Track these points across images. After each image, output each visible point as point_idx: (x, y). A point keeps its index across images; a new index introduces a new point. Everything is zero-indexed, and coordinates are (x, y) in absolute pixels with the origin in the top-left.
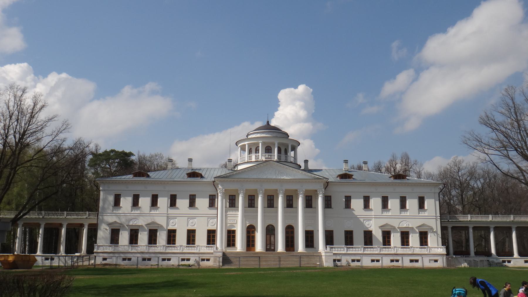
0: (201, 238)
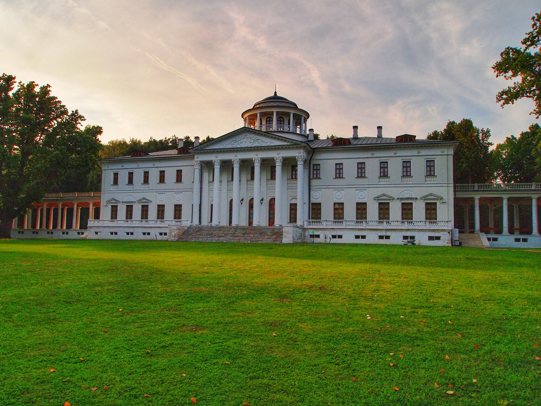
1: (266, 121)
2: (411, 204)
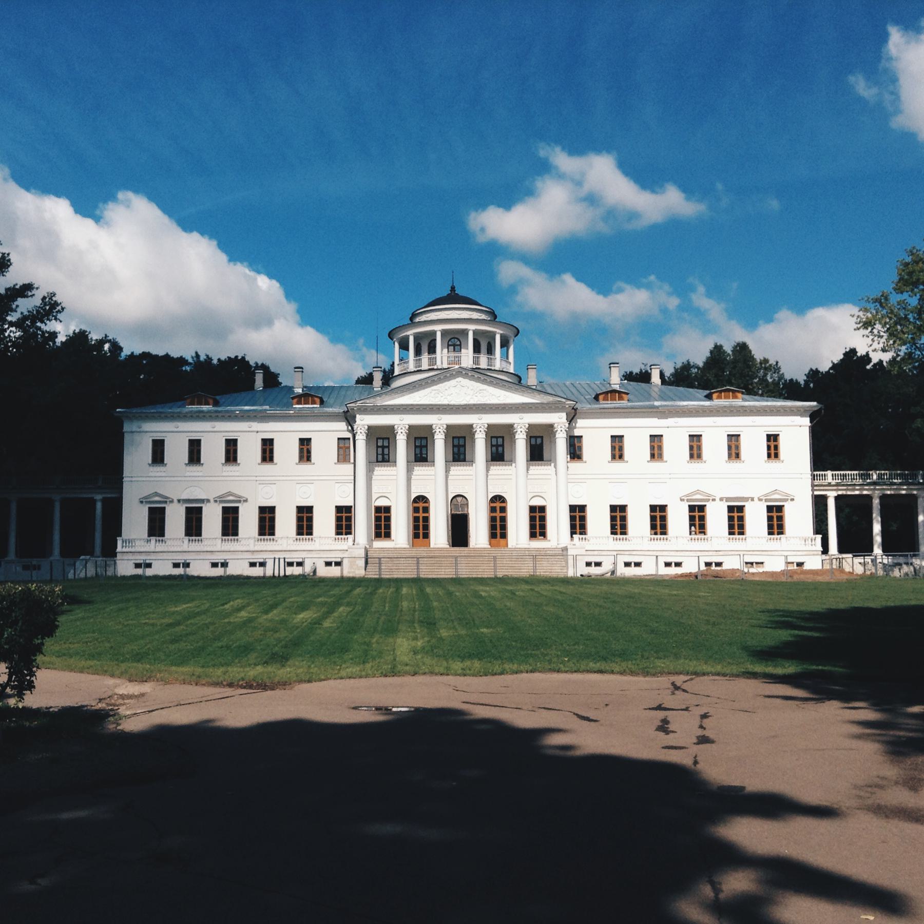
0: (324, 522)
1: (449, 345)
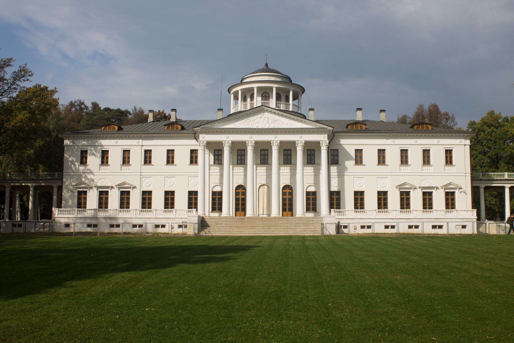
2: (129, 192)
